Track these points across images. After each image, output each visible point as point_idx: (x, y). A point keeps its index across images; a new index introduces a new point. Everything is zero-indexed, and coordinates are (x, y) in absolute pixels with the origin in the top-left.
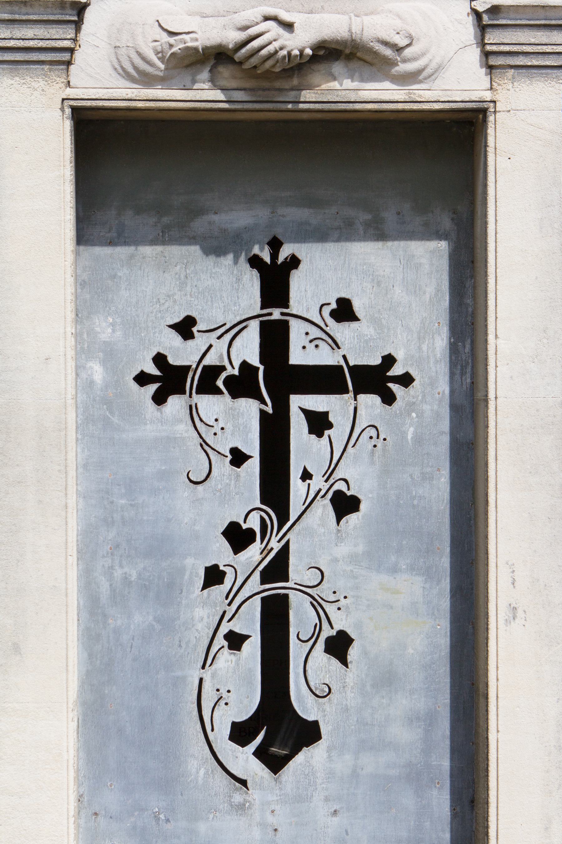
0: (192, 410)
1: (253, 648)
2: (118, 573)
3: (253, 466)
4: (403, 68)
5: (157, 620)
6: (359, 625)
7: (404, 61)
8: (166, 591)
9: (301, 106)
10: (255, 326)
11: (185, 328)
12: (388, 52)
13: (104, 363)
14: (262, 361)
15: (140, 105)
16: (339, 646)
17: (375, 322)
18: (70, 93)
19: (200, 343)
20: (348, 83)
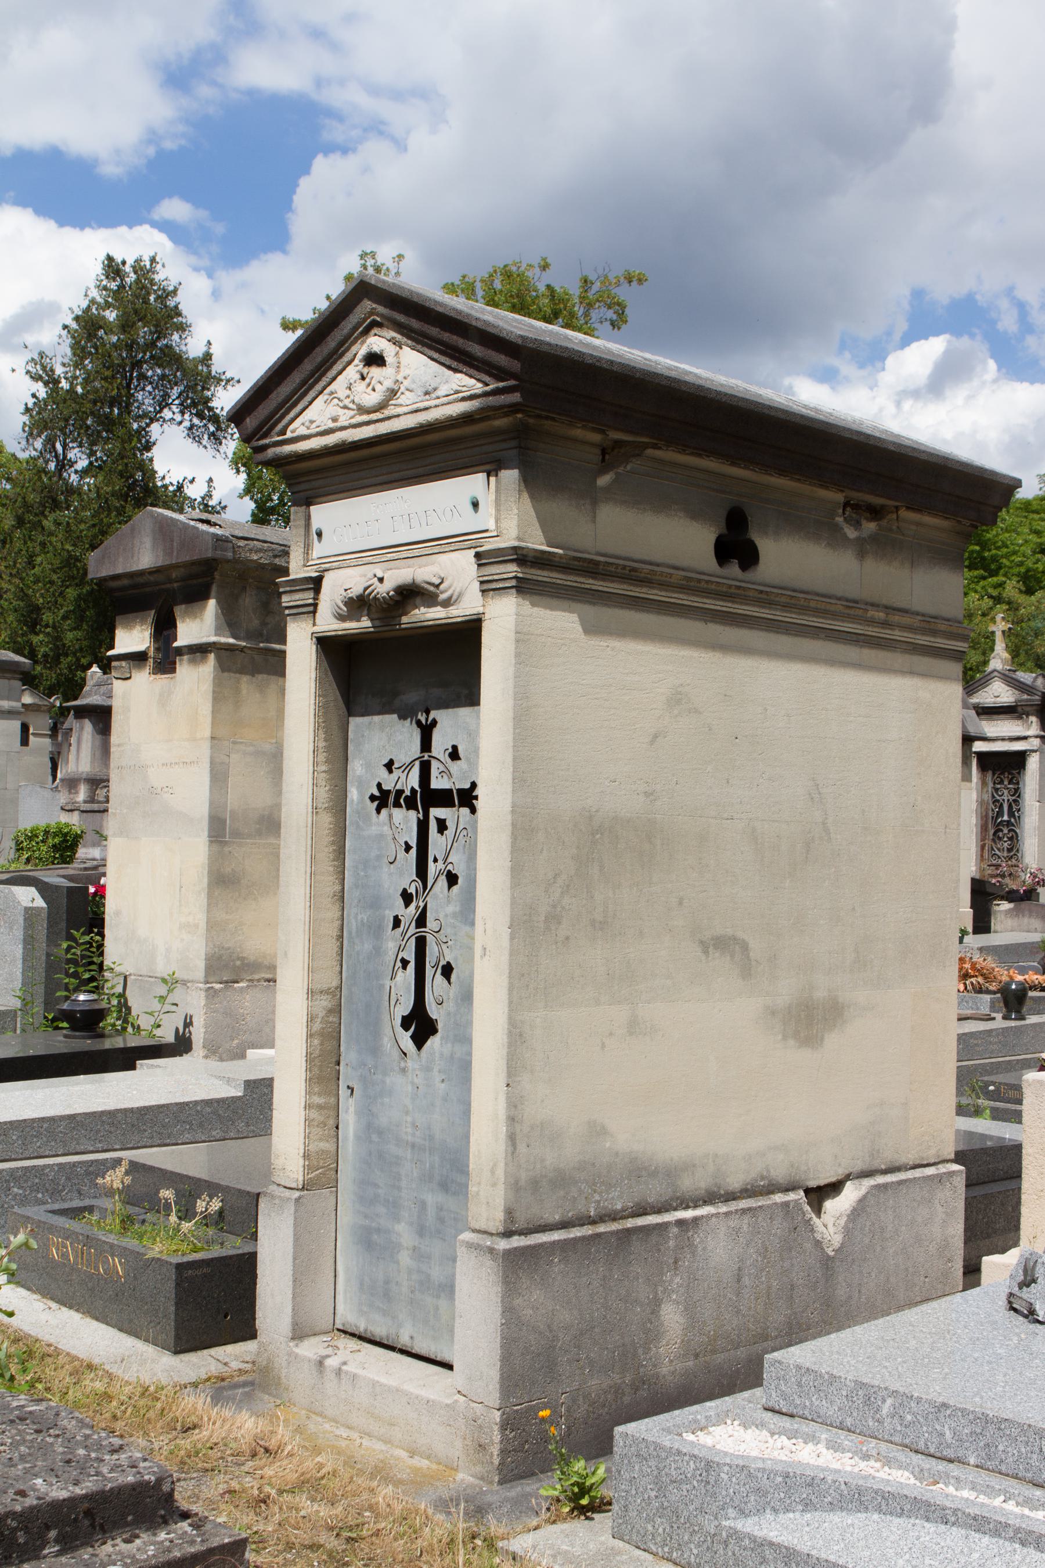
0: (390, 816)
1: (411, 967)
2: (359, 917)
3: (413, 852)
4: (443, 597)
5: (374, 947)
6: (456, 959)
7: (442, 593)
8: (376, 931)
9: (403, 626)
10: (417, 763)
11: (389, 766)
12: (432, 588)
13: (358, 788)
14: (420, 786)
15: (340, 633)
16: (447, 971)
17: (468, 759)
18: (316, 629)
19: (396, 773)
20: (423, 610)
